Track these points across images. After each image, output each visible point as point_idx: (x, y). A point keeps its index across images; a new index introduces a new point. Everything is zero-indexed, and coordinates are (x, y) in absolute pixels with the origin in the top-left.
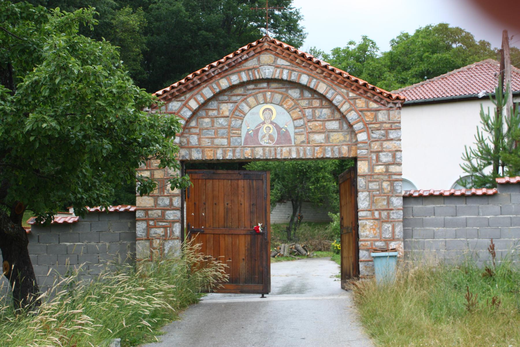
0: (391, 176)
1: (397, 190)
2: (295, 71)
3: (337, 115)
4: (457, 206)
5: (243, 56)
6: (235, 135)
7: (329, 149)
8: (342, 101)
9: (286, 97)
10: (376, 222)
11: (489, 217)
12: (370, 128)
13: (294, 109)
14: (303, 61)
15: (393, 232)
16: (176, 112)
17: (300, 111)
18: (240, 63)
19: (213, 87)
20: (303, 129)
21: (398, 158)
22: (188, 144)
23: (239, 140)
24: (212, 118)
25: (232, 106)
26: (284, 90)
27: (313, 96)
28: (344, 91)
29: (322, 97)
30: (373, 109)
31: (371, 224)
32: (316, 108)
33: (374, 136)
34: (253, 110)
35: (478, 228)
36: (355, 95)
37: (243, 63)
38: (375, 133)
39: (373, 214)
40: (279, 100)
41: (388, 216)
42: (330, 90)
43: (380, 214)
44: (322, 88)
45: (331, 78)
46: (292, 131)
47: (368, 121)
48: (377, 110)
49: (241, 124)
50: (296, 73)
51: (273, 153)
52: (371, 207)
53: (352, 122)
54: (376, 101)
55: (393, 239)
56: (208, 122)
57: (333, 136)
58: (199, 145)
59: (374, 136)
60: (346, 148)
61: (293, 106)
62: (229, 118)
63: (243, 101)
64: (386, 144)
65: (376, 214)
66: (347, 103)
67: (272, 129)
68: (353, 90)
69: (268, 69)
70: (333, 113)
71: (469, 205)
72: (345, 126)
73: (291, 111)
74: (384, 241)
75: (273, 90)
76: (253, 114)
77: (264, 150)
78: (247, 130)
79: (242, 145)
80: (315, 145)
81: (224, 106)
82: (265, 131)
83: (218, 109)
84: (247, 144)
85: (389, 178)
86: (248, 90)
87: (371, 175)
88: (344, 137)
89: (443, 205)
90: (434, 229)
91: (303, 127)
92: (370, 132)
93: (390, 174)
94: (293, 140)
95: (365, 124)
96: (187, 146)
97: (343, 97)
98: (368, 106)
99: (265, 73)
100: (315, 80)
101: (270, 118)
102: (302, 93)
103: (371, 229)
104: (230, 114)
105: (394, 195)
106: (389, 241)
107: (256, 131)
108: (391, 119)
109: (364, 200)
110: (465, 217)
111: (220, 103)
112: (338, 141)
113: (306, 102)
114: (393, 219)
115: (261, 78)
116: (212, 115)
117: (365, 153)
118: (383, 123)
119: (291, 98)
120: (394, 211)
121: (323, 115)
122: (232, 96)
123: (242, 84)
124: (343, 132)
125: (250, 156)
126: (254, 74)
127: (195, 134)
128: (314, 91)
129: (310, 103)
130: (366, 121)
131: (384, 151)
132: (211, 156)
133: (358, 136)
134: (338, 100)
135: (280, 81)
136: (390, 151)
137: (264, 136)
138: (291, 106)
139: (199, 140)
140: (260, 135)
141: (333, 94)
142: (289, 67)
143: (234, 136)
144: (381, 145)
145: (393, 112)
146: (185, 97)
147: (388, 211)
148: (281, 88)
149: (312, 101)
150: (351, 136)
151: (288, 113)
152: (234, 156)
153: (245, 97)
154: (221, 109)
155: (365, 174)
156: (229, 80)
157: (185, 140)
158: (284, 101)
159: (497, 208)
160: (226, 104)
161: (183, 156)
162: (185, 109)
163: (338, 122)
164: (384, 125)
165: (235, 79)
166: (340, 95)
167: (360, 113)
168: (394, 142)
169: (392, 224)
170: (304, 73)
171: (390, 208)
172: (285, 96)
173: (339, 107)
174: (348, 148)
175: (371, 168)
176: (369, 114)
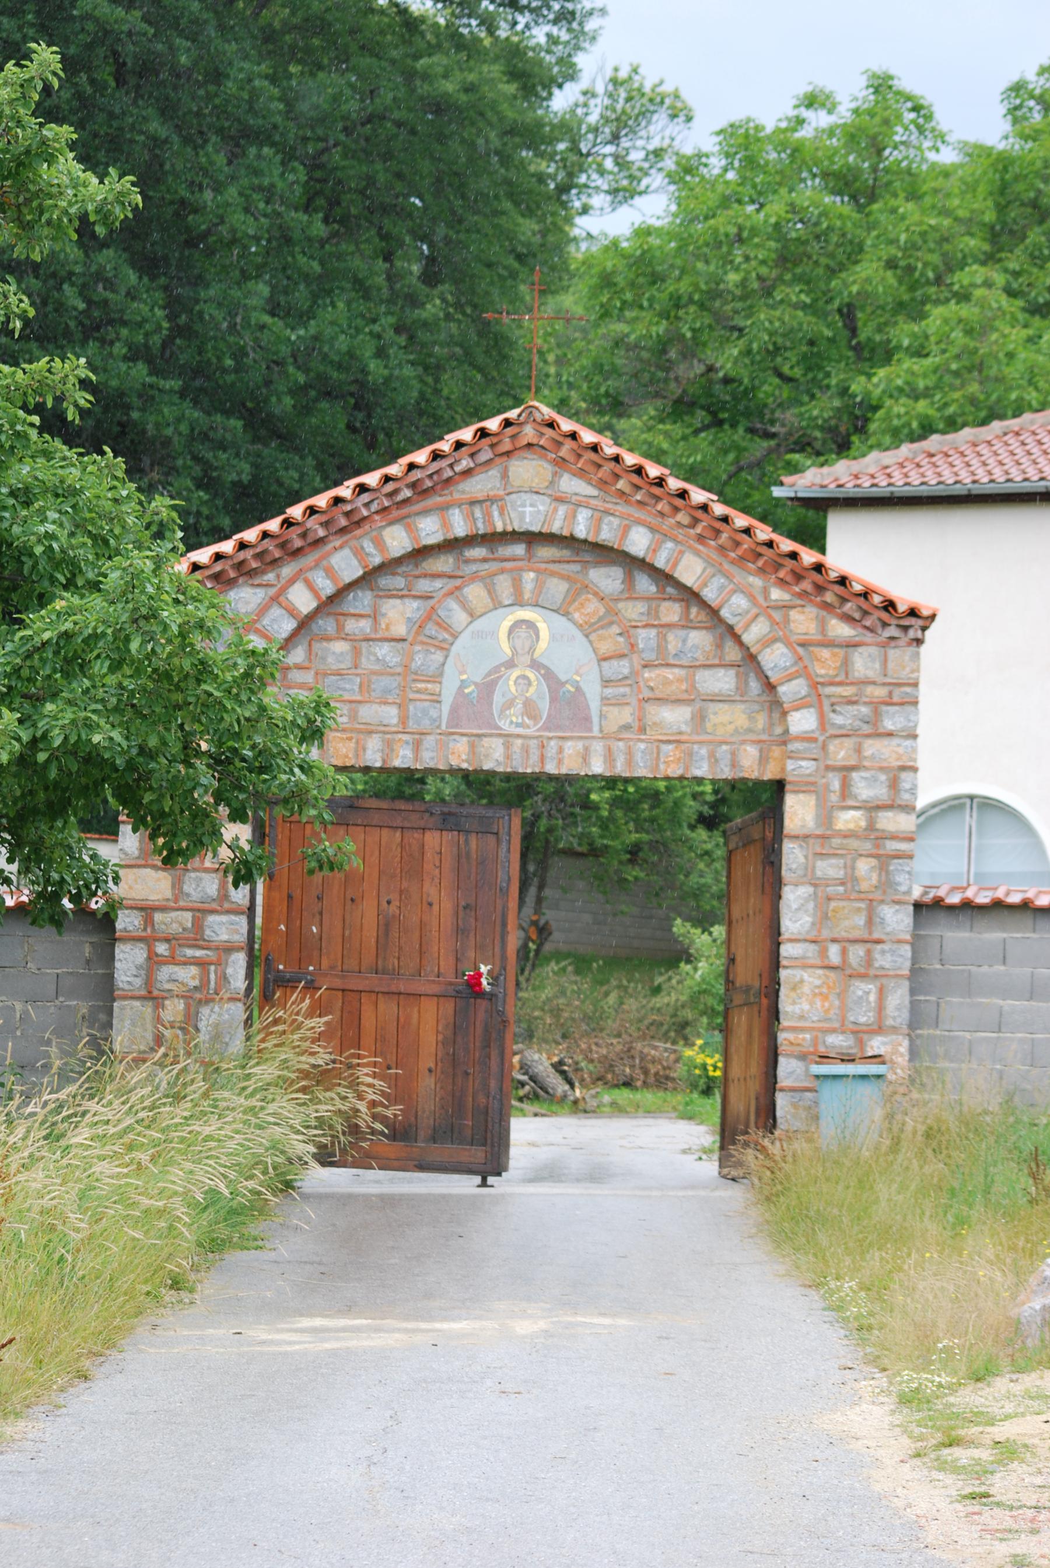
1: (899, 884)
2: (612, 514)
3: (733, 653)
5: (457, 461)
6: (423, 697)
7: (704, 751)
8: (747, 612)
9: (580, 589)
12: (828, 696)
13: (602, 627)
14: (638, 488)
15: (881, 1008)
17: (620, 634)
19: (362, 548)
20: (627, 690)
21: (906, 791)
23: (433, 713)
25: (418, 609)
27: (661, 590)
28: (756, 582)
29: (690, 596)
31: (818, 982)
32: (669, 626)
33: (839, 720)
36: (786, 596)
38: (841, 713)
39: (823, 953)
40: (559, 598)
42: (714, 575)
43: (844, 952)
46: (593, 691)
49: (443, 664)
51: (534, 757)
52: (819, 931)
54: (848, 618)
55: (880, 1028)
57: (715, 713)
59: (839, 720)
61: (600, 619)
62: (405, 645)
63: (450, 593)
64: (871, 747)
65: (834, 951)
66: (761, 619)
69: (532, 505)
70: (720, 646)
75: (543, 566)
77: (507, 746)
78: (458, 684)
79: (444, 727)
81: (394, 607)
82: (513, 689)
83: (375, 616)
84: (457, 726)
86: (467, 561)
87: (823, 837)
88: (751, 718)
91: (629, 682)
92: (827, 708)
94: (595, 719)
100: (670, 545)
101: (532, 650)
103: (815, 995)
104: (409, 632)
106: (864, 1032)
107: (488, 688)
109: (798, 909)
112: (730, 728)
113: (641, 607)
115: (509, 529)
116: (357, 632)
117: (808, 772)
119: (596, 594)
122: (417, 577)
123: (451, 545)
126: (488, 516)
128: (664, 578)
131: (866, 768)
133: (789, 718)
135: (569, 541)
136: (881, 769)
137: (510, 704)
140: (498, 699)
141: (722, 588)
144: (859, 750)
147: (869, 945)
150: (770, 717)
151: (584, 639)
153: (458, 582)
154: (384, 615)
155: (805, 831)
156: (410, 529)
158: (574, 601)
160: (398, 601)
162: (276, 612)
163: (732, 672)
164: (869, 689)
167: (800, 650)
168: (895, 741)
169: (878, 984)
170: (639, 522)
171: (876, 936)
172: (579, 585)
174: (761, 751)
175: (826, 816)
176: (825, 653)
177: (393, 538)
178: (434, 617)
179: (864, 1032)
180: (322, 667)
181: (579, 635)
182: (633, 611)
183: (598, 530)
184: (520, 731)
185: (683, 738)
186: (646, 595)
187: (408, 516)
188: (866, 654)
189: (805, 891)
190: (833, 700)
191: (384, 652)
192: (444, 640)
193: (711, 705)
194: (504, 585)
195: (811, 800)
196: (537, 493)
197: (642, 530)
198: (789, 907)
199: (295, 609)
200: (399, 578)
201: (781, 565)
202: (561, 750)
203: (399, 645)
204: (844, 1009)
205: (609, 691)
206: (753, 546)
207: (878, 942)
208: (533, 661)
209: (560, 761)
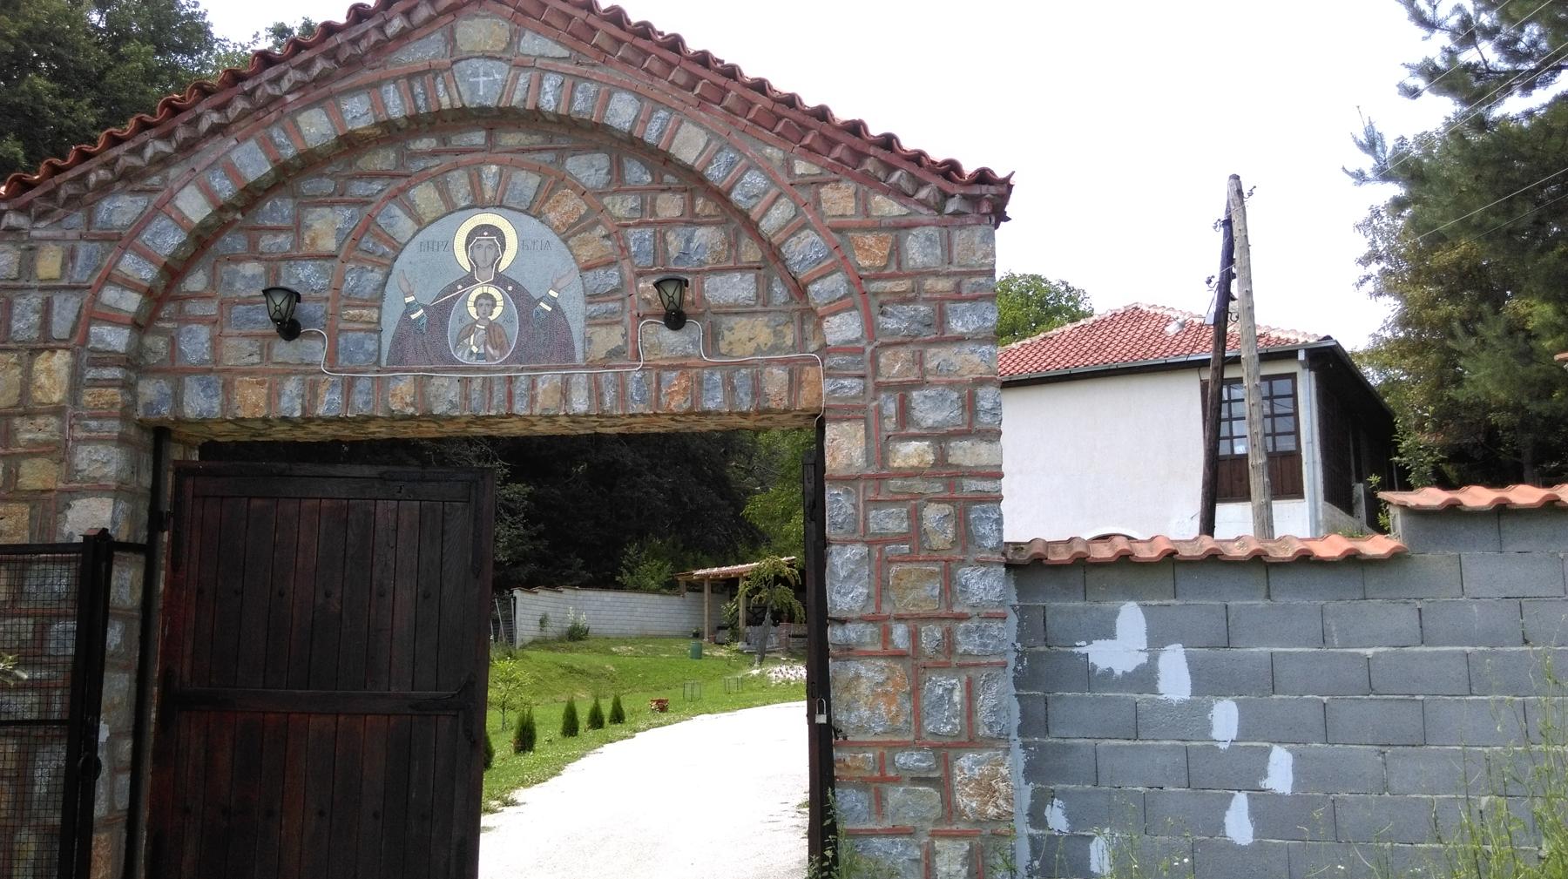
0: (957, 481)
1: (984, 537)
2: (588, 79)
3: (751, 252)
4: (1232, 604)
5: (388, 21)
6: (356, 326)
7: (717, 377)
8: (766, 192)
9: (555, 183)
10: (898, 667)
11: (1370, 652)
12: (876, 294)
13: (584, 230)
14: (619, 42)
15: (970, 710)
16: (126, 233)
17: (607, 237)
18: (380, 48)
19: (271, 138)
20: (616, 306)
21: (986, 412)
22: (173, 360)
23: (370, 346)
24: (272, 260)
25: (352, 218)
26: (548, 157)
27: (658, 179)
28: (775, 153)
29: (692, 180)
30: (885, 222)
31: (880, 678)
32: (670, 223)
33: (891, 324)
34: (432, 232)
35: (1325, 699)
36: (815, 170)
37: (392, 52)
38: (893, 315)
39: (886, 636)
40: (530, 193)
41: (948, 644)
42: (720, 150)
43: (914, 636)
44: (690, 145)
45: (725, 103)
46: (576, 311)
47: (865, 269)
48: (902, 227)
49: (384, 284)
50: (592, 88)
51: (499, 393)
52: (878, 607)
53: (803, 274)
54: (898, 193)
55: (971, 740)
56: (254, 276)
57: (731, 329)
58: (215, 362)
59: (891, 324)
60: (779, 375)
61: (581, 219)
62: (336, 263)
63: (392, 197)
64: (936, 357)
65: (900, 633)
66: (784, 200)
67: (500, 303)
68: (809, 148)
69: (486, 74)
70: (733, 244)
71: (1281, 601)
72: (779, 292)
73: (574, 235)
74: (933, 747)
75: (508, 156)
76: (428, 246)
77: (465, 382)
78: (402, 309)
79: (384, 363)
80: (661, 363)
81: (323, 217)
82: (472, 311)
83: (297, 228)
84: (400, 362)
85: (950, 487)
86: (415, 155)
87: (879, 478)
88: (776, 333)
89: (1173, 601)
90: (1138, 697)
91: (620, 296)
92: (875, 310)
93: (959, 474)
94: (578, 346)
95: (859, 279)
96: (167, 365)
97: (772, 179)
98: (866, 213)
99: (474, 88)
100: (662, 114)
101: (496, 261)
102: (617, 170)
103: (876, 696)
104: (340, 246)
105: (971, 559)
106: (949, 747)
107: (440, 312)
108: (956, 261)
109: (849, 576)
110: (1263, 650)
111: (306, 205)
112: (751, 346)
113: (631, 202)
114: (967, 654)
115: (458, 104)
116: (274, 249)
117: (853, 392)
118: (921, 274)
119: (574, 188)
120: (972, 625)
121: (696, 252)
122: (352, 178)
123: (390, 133)
124: (772, 315)
125: (412, 404)
126: (430, 92)
127: (201, 320)
128: (660, 159)
129: (648, 207)
130: (861, 268)
131: (931, 385)
132: (257, 406)
133: (825, 325)
134: (750, 187)
135: (531, 118)
136: (951, 385)
137: (471, 328)
138: (576, 217)
139: (215, 342)
140: (453, 325)
141: (731, 164)
142: (563, 66)
143: (352, 330)
144: (920, 361)
145: (965, 233)
146: (165, 180)
147: (947, 624)
148: (540, 150)
149: (654, 200)
150: (802, 330)
151: (563, 245)
152: (347, 404)
153: (403, 182)
154: (309, 227)
155: (853, 471)
156: (336, 115)
157: (161, 344)
158: (548, 198)
159: (1402, 617)
160: (327, 211)
161: (149, 406)
162: (161, 223)
163: (750, 276)
164: (930, 283)
165: (357, 112)
166: (759, 168)
167: (835, 236)
168: (967, 348)
169: (964, 678)
170: (622, 88)
171: (957, 610)
172: (553, 178)
173: (754, 215)
174: (791, 373)
175: (879, 450)
176: (870, 239)
177: (311, 125)
178: (372, 227)
179: (949, 747)
180: (229, 295)
181: (556, 240)
182: (622, 206)
183: (571, 101)
184: (482, 363)
185: (690, 362)
186: (639, 186)
187: (330, 96)
188: (922, 238)
189: (854, 552)
190: (882, 298)
191: (307, 272)
192: (383, 255)
193: (724, 319)
194: (459, 185)
195: (858, 430)
196: (491, 58)
197: (626, 97)
198: (835, 574)
199: (184, 217)
200: (326, 180)
201: (807, 129)
202: (533, 386)
203: (328, 264)
204: (917, 713)
205: (592, 308)
206: (769, 104)
207: (961, 618)
208: (497, 274)
209: (533, 399)
